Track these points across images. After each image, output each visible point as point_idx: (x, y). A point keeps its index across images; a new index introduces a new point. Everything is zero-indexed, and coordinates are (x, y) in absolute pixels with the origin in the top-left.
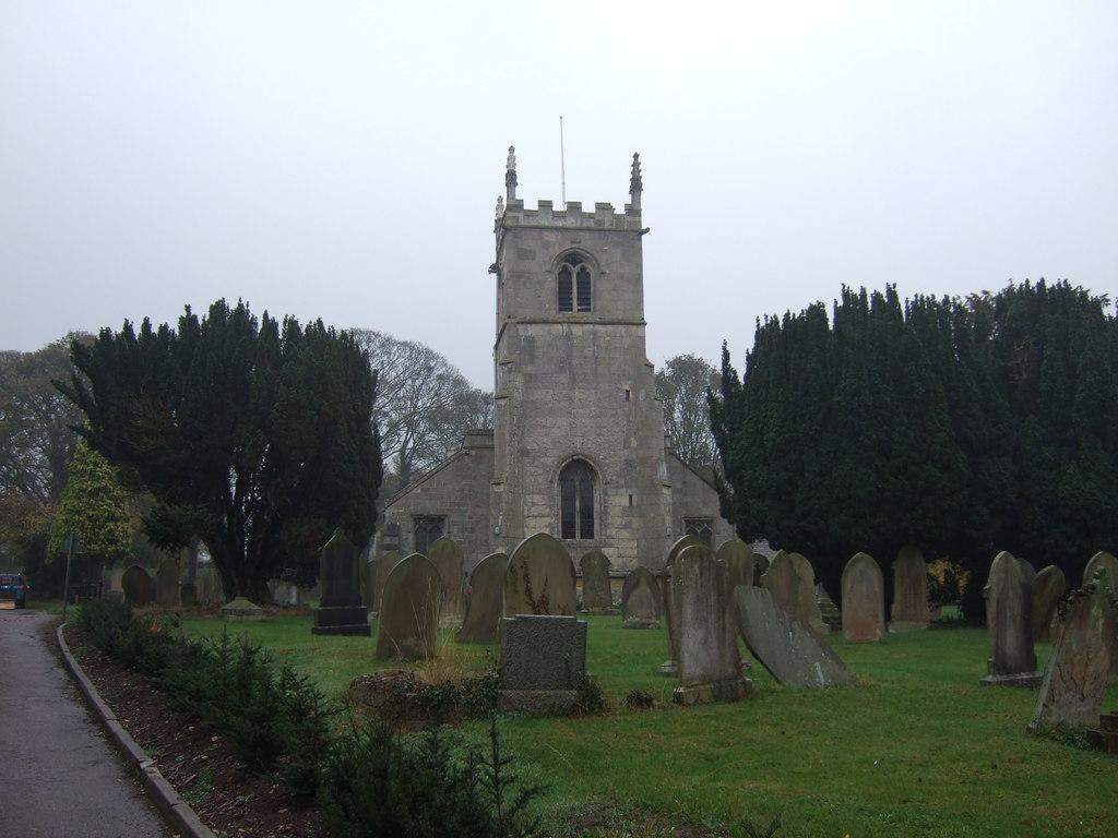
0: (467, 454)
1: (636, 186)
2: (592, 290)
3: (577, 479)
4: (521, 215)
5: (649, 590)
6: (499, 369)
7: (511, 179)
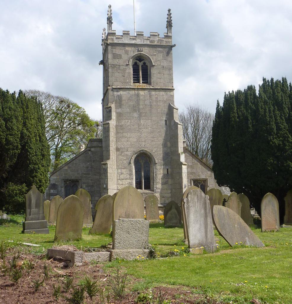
0: (89, 150)
1: (169, 25)
2: (149, 73)
3: (142, 162)
4: (114, 38)
5: (176, 211)
6: (104, 109)
7: (110, 20)
